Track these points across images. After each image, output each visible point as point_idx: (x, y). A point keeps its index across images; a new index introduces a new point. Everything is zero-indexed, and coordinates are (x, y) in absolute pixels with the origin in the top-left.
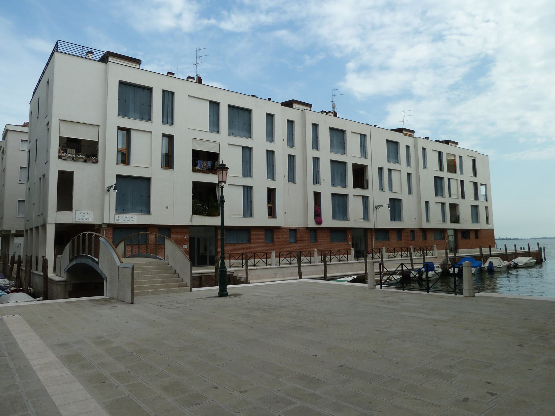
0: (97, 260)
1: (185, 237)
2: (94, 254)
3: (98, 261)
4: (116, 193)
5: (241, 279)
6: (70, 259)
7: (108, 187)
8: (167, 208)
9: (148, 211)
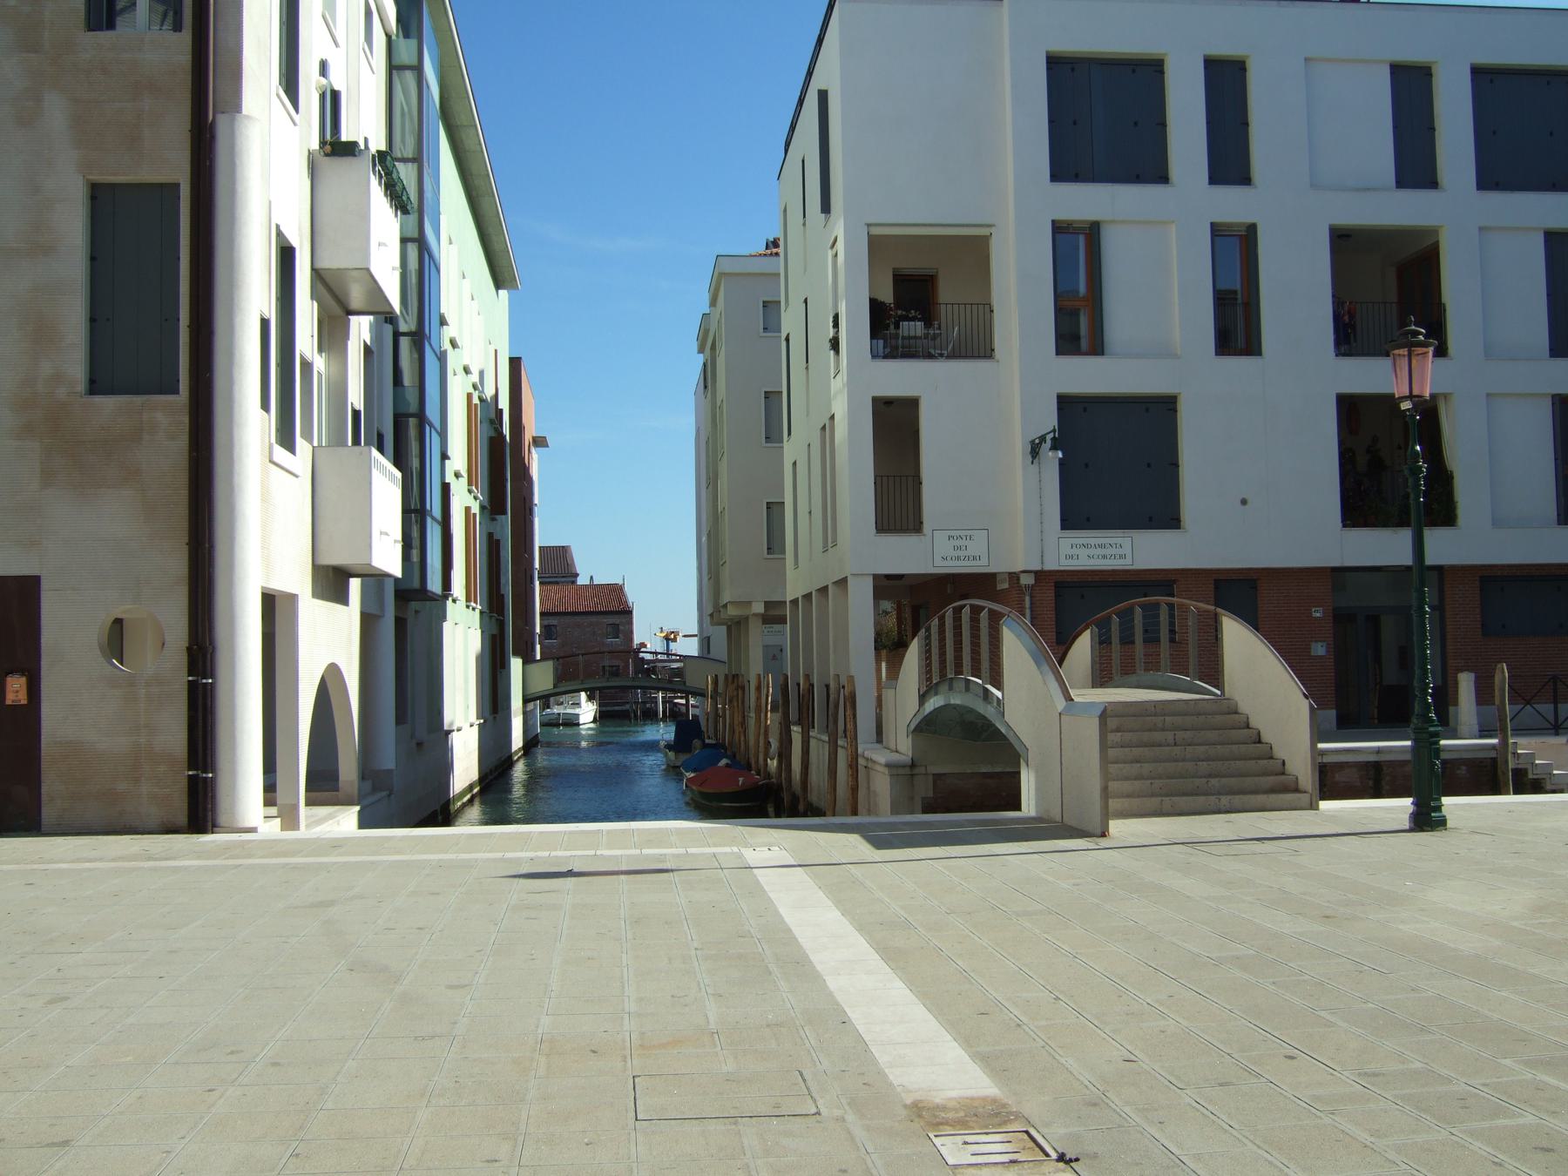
0: (998, 694)
1: (1318, 615)
2: (988, 675)
3: (1000, 696)
4: (1060, 459)
5: (1548, 781)
6: (921, 693)
7: (1032, 442)
8: (1244, 502)
9: (1170, 519)
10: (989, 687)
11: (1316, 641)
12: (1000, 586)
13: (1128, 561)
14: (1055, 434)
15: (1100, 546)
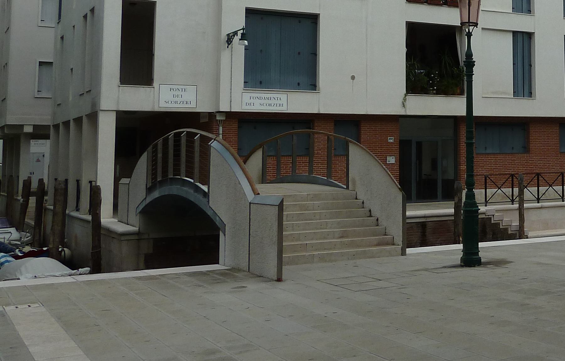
0: (205, 188)
1: (391, 141)
3: (206, 190)
4: (246, 46)
5: (509, 229)
6: (148, 187)
7: (228, 35)
9: (313, 86)
10: (198, 184)
11: (391, 156)
12: (202, 121)
13: (193, 105)
14: (243, 31)
15: (268, 99)
